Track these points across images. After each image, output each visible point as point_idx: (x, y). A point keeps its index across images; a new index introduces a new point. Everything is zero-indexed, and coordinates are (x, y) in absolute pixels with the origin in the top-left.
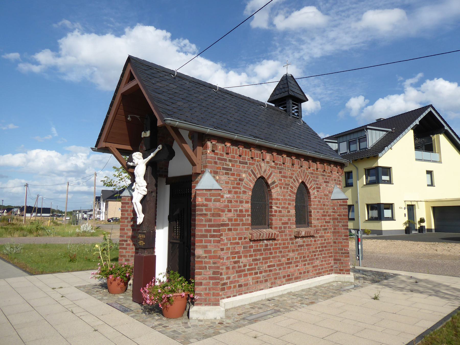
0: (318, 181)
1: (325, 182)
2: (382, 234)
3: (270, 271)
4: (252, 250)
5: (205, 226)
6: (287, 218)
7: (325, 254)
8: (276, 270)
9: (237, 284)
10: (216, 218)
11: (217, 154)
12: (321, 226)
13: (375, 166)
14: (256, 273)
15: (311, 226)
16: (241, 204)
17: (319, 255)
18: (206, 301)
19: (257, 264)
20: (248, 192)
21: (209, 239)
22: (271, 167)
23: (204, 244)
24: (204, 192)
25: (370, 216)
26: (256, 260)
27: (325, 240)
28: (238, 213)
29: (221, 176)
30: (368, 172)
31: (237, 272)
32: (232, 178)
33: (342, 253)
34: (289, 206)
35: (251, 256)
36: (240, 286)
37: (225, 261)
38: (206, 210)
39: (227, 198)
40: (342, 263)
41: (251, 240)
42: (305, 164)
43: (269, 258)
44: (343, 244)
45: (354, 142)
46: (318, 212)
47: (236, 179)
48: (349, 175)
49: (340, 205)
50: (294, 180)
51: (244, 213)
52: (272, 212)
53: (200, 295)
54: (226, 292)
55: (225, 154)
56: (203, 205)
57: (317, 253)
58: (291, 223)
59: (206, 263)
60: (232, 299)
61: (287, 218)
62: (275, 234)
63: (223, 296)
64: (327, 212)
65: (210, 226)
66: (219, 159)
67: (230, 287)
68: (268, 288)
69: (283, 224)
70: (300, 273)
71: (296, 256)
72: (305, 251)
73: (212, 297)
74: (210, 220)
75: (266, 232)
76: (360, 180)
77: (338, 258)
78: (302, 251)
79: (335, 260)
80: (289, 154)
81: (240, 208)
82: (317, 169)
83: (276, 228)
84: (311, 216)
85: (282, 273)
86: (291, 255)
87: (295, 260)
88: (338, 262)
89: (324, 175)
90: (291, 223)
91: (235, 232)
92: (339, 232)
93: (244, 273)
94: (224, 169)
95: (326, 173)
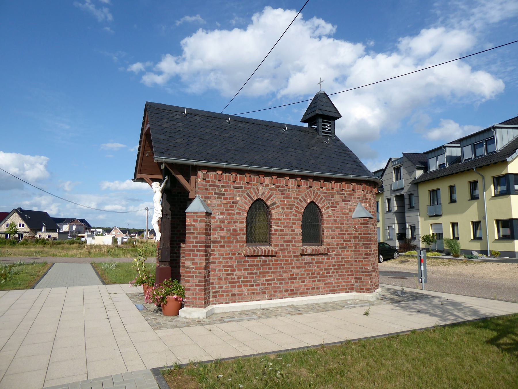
0: (334, 200)
1: (344, 201)
2: (515, 257)
3: (268, 284)
4: (247, 264)
5: (192, 242)
6: (291, 237)
7: (342, 272)
8: (276, 284)
9: (230, 294)
10: (201, 236)
11: (209, 182)
12: (338, 245)
13: (504, 172)
14: (253, 285)
15: (324, 245)
16: (235, 224)
17: (333, 272)
18: (193, 304)
19: (253, 277)
20: (243, 214)
21: (196, 253)
22: (271, 190)
23: (192, 257)
24: (192, 214)
25: (501, 234)
26: (252, 273)
27: (343, 258)
28: (232, 232)
29: (213, 201)
30: (498, 181)
31: (230, 283)
32: (225, 202)
33: (362, 272)
34: (294, 226)
35: (245, 270)
36: (234, 295)
37: (217, 273)
38: (194, 229)
39: (219, 219)
40: (362, 282)
41: (245, 256)
42: (316, 185)
43: (268, 273)
44: (364, 263)
45: (481, 145)
46: (333, 231)
47: (229, 202)
48: (474, 185)
49: (361, 224)
50: (300, 200)
51: (238, 232)
52: (271, 231)
53: (188, 298)
54: (218, 299)
55: (217, 181)
56: (191, 225)
57: (331, 271)
58: (295, 242)
59: (193, 273)
60: (224, 305)
61: (291, 237)
62: (272, 251)
63: (215, 302)
64: (347, 231)
65: (196, 242)
66: (210, 186)
67: (223, 296)
68: (266, 300)
69: (285, 242)
70: (308, 289)
71: (303, 272)
72: (315, 268)
73: (198, 301)
74: (197, 238)
75: (262, 249)
76: (487, 192)
77: (359, 276)
78: (311, 268)
79: (356, 278)
80: (293, 176)
81: (234, 227)
82: (333, 188)
83: (276, 246)
84: (323, 234)
85: (283, 287)
86: (295, 271)
87: (300, 276)
88: (359, 280)
89: (343, 194)
90: (295, 242)
91: (228, 248)
92: (359, 251)
93: (238, 284)
94: (215, 194)
95: (346, 191)
